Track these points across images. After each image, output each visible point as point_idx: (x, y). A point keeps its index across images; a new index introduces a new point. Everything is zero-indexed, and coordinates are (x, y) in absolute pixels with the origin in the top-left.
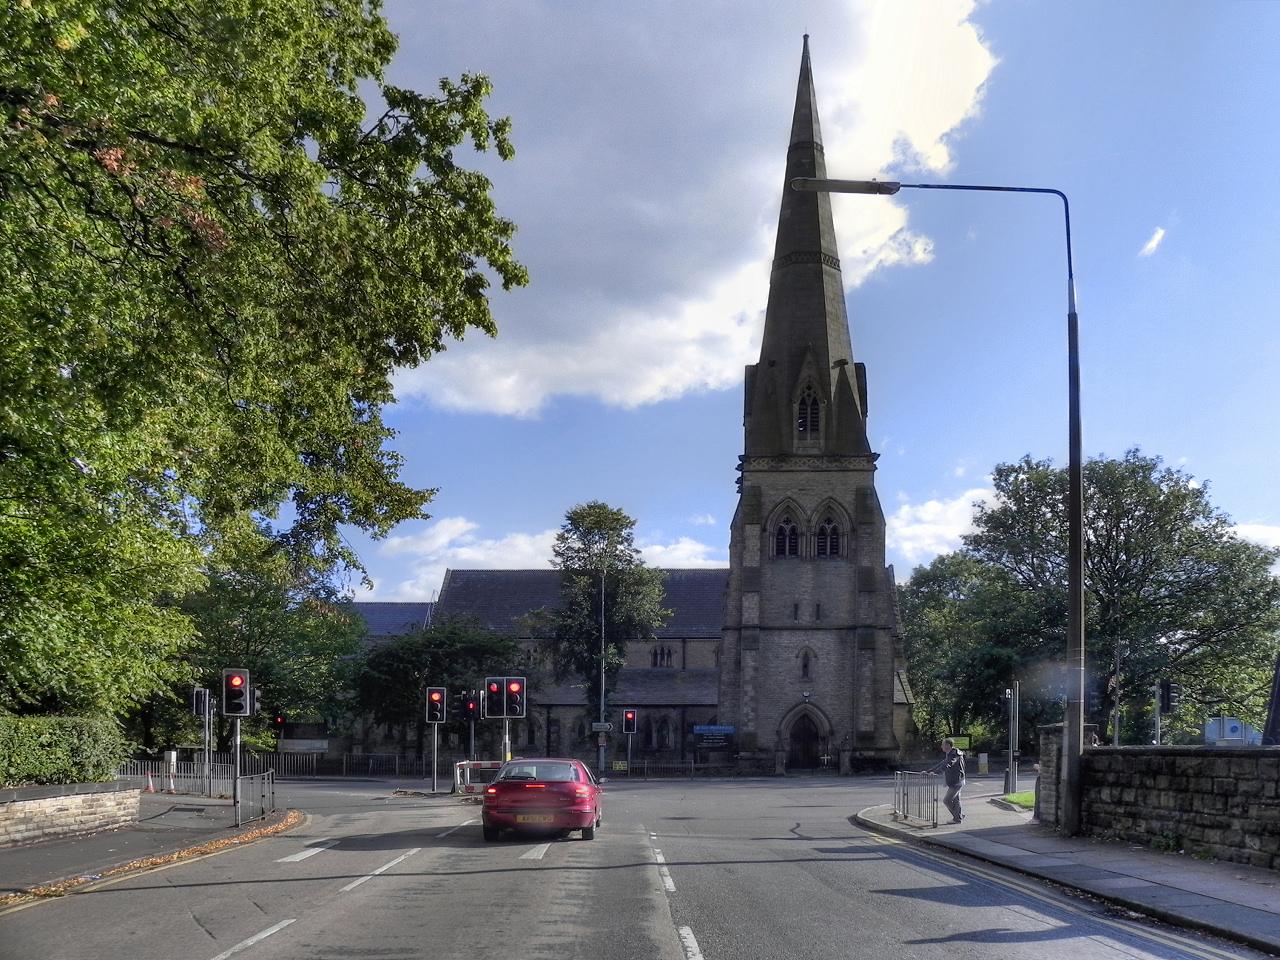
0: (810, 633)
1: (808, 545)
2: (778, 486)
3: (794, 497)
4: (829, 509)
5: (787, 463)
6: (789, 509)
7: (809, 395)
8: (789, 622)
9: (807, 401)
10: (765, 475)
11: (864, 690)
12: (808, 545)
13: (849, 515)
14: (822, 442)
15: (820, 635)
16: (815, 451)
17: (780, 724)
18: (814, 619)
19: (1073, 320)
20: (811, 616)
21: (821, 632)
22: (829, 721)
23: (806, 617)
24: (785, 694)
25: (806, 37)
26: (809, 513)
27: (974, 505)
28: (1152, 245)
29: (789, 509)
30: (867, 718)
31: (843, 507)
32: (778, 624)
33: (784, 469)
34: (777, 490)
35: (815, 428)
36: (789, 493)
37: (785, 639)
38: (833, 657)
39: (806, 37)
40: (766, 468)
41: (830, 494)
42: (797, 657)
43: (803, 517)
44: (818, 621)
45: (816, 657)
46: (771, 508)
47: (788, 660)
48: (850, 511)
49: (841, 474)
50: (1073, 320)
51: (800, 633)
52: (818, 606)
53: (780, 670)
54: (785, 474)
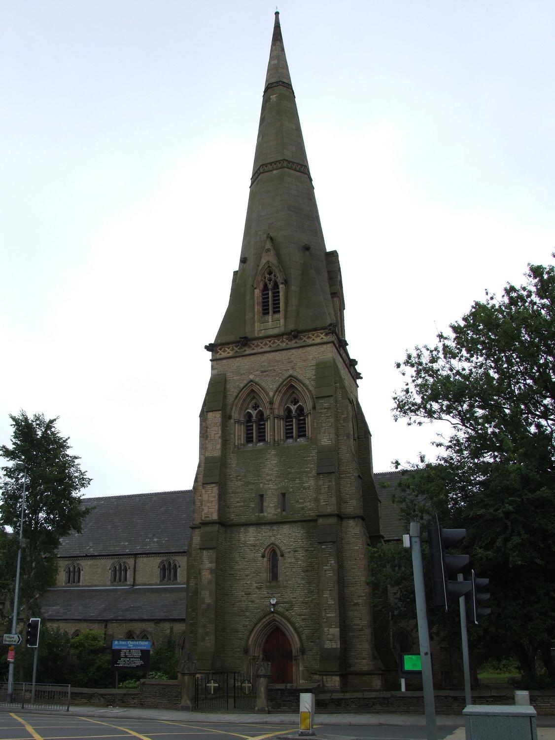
0: (275, 528)
1: (274, 429)
2: (245, 369)
3: (257, 380)
4: (290, 388)
5: (250, 347)
6: (252, 393)
7: (270, 280)
8: (253, 517)
9: (268, 285)
10: (230, 361)
11: (326, 595)
12: (274, 429)
13: (310, 391)
14: (282, 321)
15: (286, 529)
16: (276, 331)
17: (248, 638)
18: (279, 510)
19: (277, 27)
20: (276, 507)
21: (286, 527)
22: (299, 635)
23: (271, 510)
24: (252, 602)
25: (277, 14)
26: (271, 394)
27: (456, 322)
28: (549, 470)
29: (252, 393)
30: (332, 631)
31: (302, 384)
32: (243, 519)
33: (246, 353)
34: (241, 375)
35: (276, 311)
36: (252, 377)
37: (250, 536)
38: (301, 554)
39: (277, 14)
40: (231, 354)
41: (291, 372)
42: (263, 557)
43: (266, 400)
44: (284, 513)
45: (282, 555)
46: (235, 394)
47: (254, 560)
48: (311, 388)
49: (300, 351)
50: (277, 27)
51: (265, 529)
52: (284, 495)
53: (247, 572)
54: (249, 357)
